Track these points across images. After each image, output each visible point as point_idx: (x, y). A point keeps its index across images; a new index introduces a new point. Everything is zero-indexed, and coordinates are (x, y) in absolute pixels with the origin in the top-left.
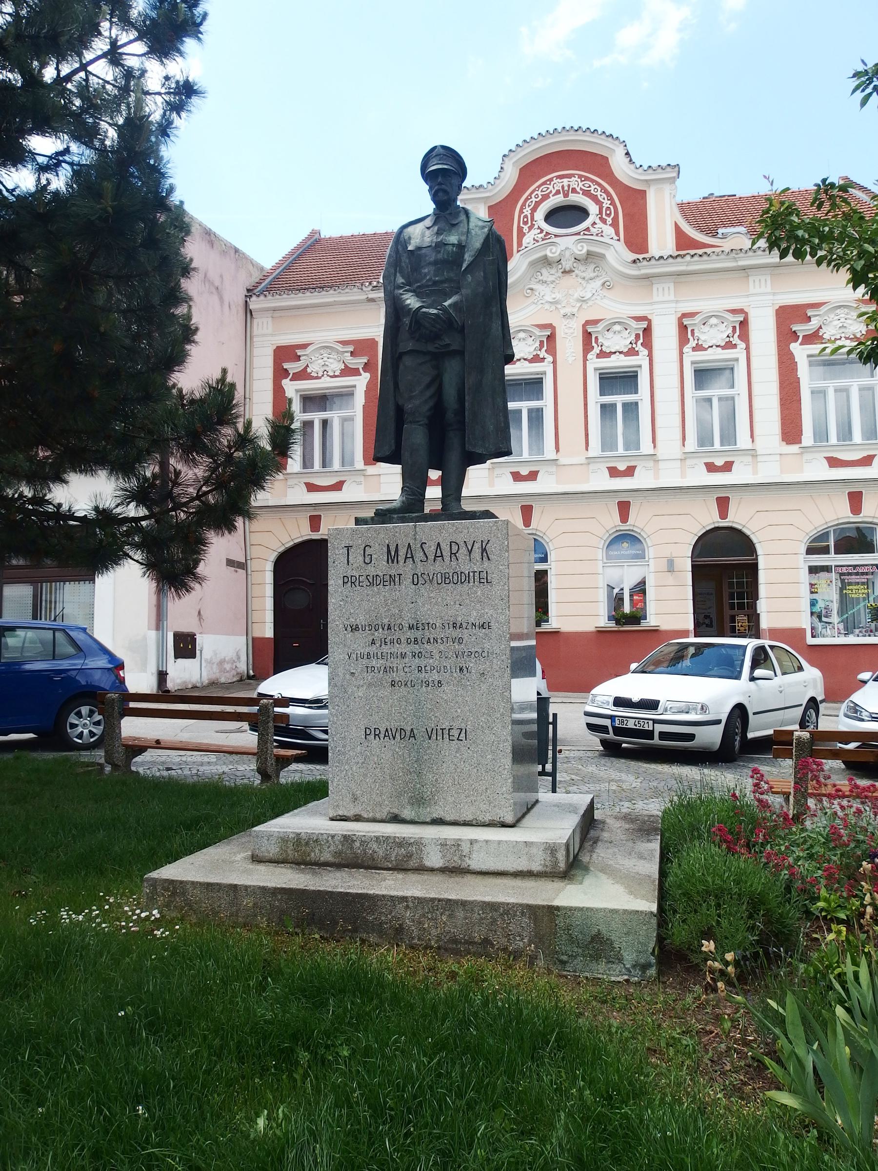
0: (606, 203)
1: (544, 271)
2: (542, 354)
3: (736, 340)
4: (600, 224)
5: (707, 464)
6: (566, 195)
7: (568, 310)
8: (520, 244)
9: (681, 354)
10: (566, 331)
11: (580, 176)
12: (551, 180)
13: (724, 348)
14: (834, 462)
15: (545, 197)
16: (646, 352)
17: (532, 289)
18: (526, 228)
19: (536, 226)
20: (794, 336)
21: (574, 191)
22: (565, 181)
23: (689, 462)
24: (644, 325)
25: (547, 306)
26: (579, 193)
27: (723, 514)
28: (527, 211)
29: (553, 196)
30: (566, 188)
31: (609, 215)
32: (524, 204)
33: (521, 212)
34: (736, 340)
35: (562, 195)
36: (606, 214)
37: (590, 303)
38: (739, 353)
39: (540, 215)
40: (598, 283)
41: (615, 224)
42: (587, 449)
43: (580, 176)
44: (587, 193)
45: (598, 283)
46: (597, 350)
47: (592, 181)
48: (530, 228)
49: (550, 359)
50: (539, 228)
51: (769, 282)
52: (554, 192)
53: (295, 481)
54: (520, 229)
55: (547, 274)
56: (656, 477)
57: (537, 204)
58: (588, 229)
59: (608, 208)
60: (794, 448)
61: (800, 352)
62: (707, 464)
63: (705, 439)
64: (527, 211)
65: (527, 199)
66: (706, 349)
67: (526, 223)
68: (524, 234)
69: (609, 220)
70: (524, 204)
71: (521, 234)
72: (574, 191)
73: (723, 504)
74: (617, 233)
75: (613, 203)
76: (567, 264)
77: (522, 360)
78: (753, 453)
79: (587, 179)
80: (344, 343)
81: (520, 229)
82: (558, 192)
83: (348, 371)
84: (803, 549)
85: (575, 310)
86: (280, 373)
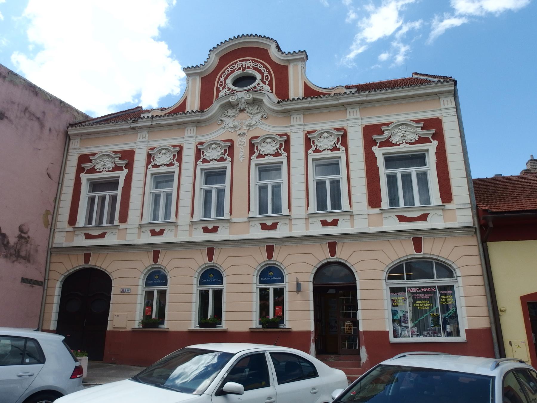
0: (266, 73)
1: (229, 111)
2: (225, 156)
3: (339, 146)
4: (262, 85)
5: (321, 221)
6: (244, 70)
7: (242, 131)
8: (217, 97)
9: (307, 154)
10: (240, 143)
11: (252, 60)
12: (236, 62)
13: (274, 155)
14: (402, 219)
15: (233, 72)
16: (286, 154)
17: (222, 121)
18: (221, 88)
19: (227, 87)
20: (374, 143)
21: (248, 68)
22: (244, 63)
23: (311, 220)
24: (285, 138)
25: (230, 130)
26: (251, 69)
27: (333, 253)
28: (222, 79)
29: (237, 71)
30: (244, 66)
31: (267, 80)
32: (221, 76)
33: (219, 79)
34: (339, 146)
35: (241, 70)
36: (266, 79)
37: (255, 127)
38: (341, 153)
39: (229, 82)
40: (259, 116)
41: (270, 84)
42: (249, 213)
43: (252, 60)
44: (255, 69)
45: (259, 116)
46: (257, 153)
47: (259, 62)
48: (223, 88)
49: (230, 159)
50: (228, 88)
51: (358, 113)
52: (237, 68)
53: (314, 219)
54: (218, 88)
55: (230, 112)
56: (176, 236)
57: (228, 75)
58: (255, 87)
59: (267, 76)
60: (377, 211)
61: (379, 152)
62: (321, 221)
63: (263, 209)
64: (222, 79)
65: (223, 73)
66: (321, 152)
67: (221, 85)
68: (220, 91)
69: (267, 82)
70: (221, 76)
71: (218, 91)
72: (248, 68)
73: (418, 244)
74: (271, 89)
75: (270, 73)
76: (242, 106)
77: (214, 160)
78: (351, 214)
79: (256, 61)
80: (417, 121)
81: (218, 88)
82: (239, 69)
83: (422, 140)
84: (384, 276)
85: (246, 131)
86: (80, 170)
